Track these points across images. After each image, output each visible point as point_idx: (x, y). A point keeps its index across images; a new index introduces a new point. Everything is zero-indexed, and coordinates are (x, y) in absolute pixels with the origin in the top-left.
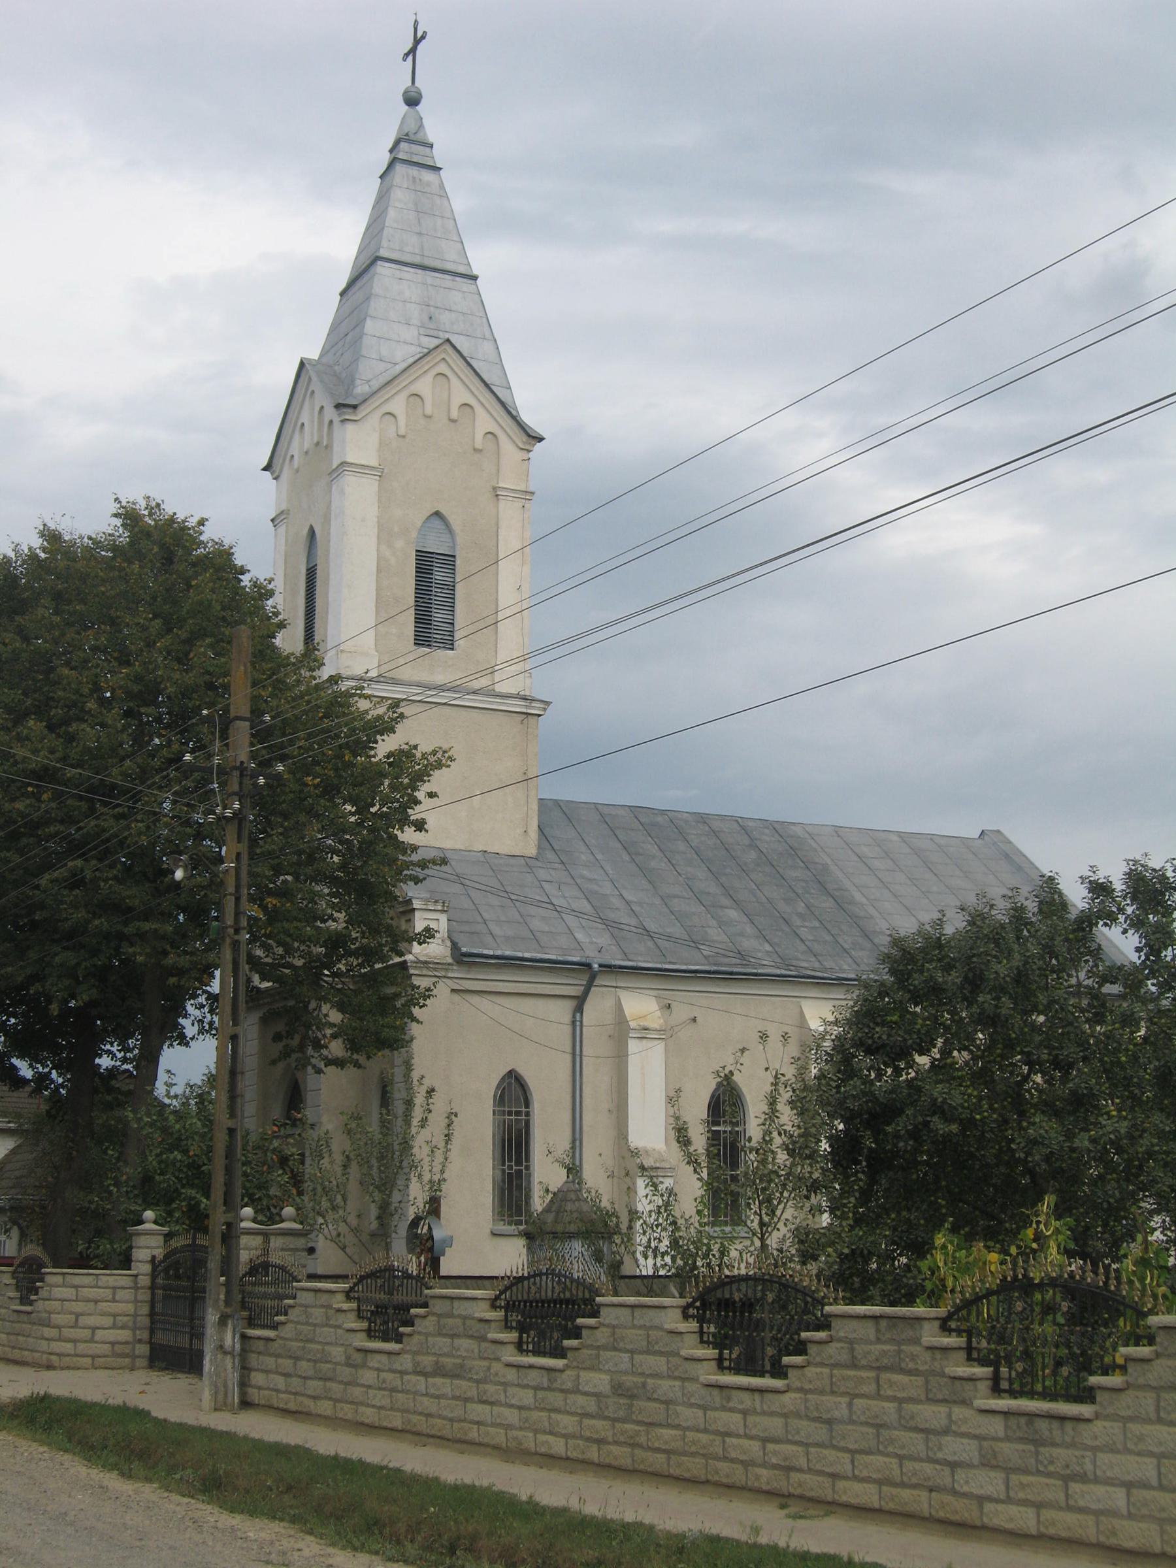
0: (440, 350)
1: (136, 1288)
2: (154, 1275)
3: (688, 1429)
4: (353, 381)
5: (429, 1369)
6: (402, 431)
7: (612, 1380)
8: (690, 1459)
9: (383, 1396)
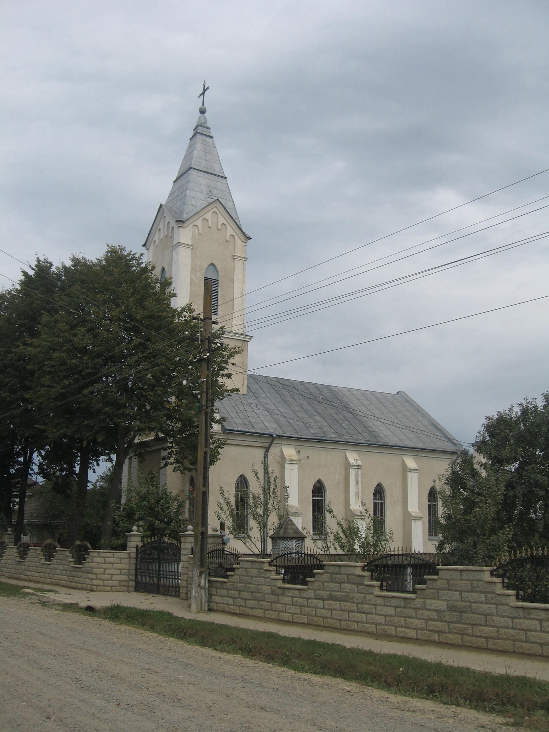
0: (214, 203)
1: (130, 558)
2: (137, 553)
3: (501, 627)
4: (182, 213)
5: (325, 597)
6: (200, 232)
7: (448, 604)
8: (503, 641)
9: (295, 608)
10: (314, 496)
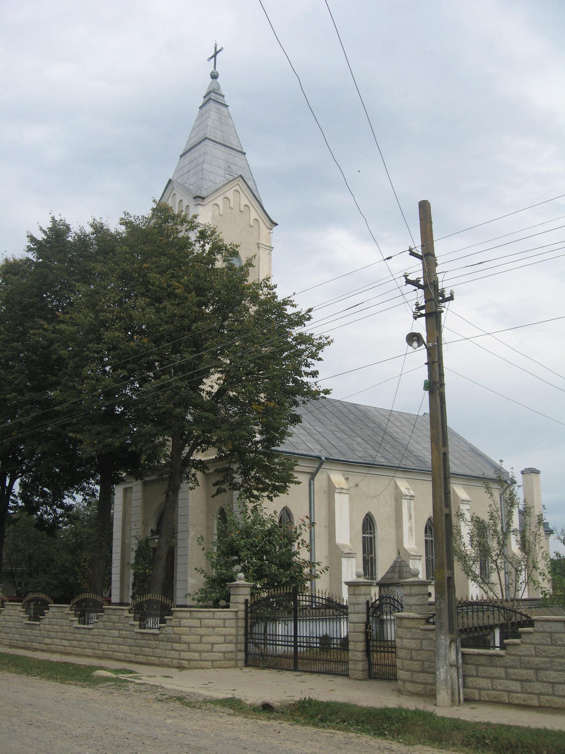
1: (237, 619)
6: (221, 213)
10: (364, 533)
